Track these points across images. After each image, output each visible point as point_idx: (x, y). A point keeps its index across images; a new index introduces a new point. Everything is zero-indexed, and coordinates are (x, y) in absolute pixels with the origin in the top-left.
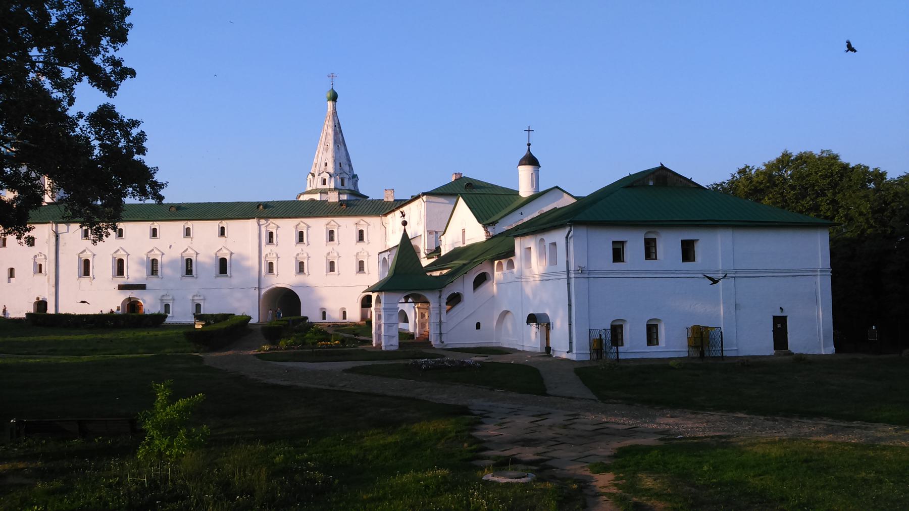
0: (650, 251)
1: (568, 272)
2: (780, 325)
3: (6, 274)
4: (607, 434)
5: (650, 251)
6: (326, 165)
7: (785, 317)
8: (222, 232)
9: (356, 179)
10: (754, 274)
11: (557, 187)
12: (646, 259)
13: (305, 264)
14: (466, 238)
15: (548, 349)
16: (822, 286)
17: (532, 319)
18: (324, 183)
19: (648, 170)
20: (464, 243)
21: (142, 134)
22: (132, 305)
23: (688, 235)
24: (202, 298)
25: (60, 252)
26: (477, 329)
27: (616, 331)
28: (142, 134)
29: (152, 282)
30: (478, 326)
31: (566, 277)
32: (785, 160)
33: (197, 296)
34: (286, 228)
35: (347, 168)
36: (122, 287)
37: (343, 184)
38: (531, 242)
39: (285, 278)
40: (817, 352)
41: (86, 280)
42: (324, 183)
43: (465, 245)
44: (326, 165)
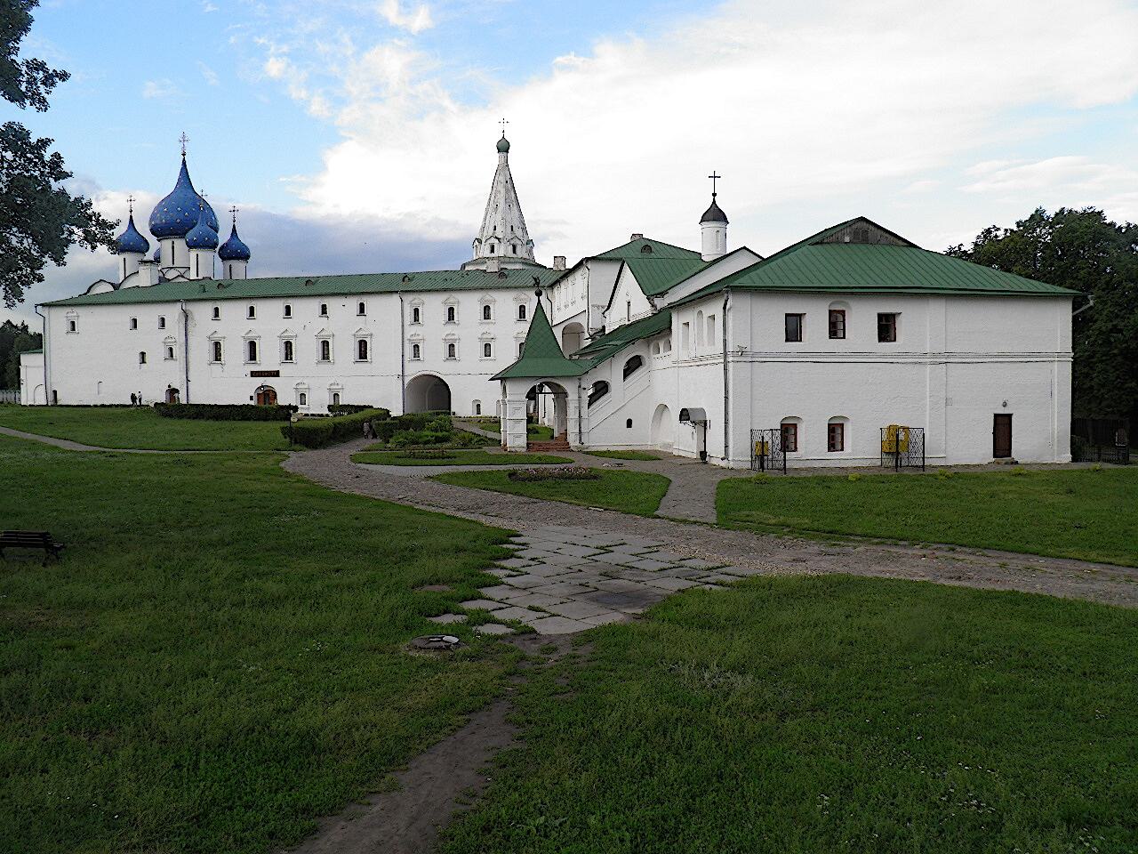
0: (836, 328)
1: (725, 354)
2: (1003, 425)
3: (138, 358)
5: (836, 328)
6: (495, 229)
7: (1010, 416)
8: (288, 310)
9: (531, 245)
10: (968, 360)
11: (745, 248)
12: (830, 338)
13: (76, 323)
14: (632, 314)
15: (703, 454)
16: (1060, 377)
17: (685, 415)
18: (492, 251)
21: (57, 156)
22: (267, 394)
23: (888, 307)
24: (306, 386)
25: (190, 334)
27: (788, 432)
28: (57, 156)
29: (284, 370)
30: (629, 423)
32: (1038, 218)
33: (334, 384)
34: (433, 306)
35: (519, 233)
36: (254, 374)
37: (514, 252)
38: (690, 316)
39: (433, 363)
40: (1056, 460)
41: (216, 367)
42: (492, 251)
44: (495, 229)
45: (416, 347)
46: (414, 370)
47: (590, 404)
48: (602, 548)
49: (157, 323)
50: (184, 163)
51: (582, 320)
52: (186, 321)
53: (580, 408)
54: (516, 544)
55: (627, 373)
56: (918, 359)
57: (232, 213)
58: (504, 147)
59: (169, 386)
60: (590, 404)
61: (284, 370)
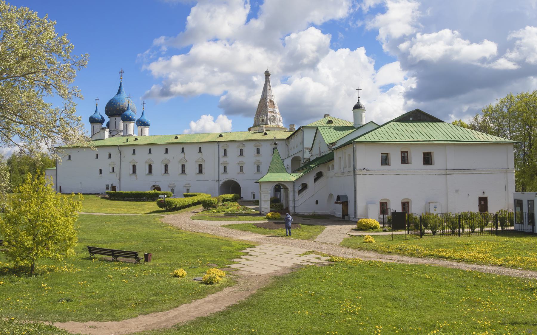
3: (98, 172)
4: (313, 263)
11: (372, 122)
12: (402, 163)
19: (411, 112)
20: (320, 155)
26: (316, 204)
30: (317, 202)
31: (353, 174)
43: (321, 156)
45: (225, 168)
46: (224, 178)
47: (299, 194)
48: (304, 260)
49: (108, 156)
50: (121, 82)
51: (301, 155)
52: (120, 155)
53: (294, 195)
54: (412, 255)
55: (316, 180)
56: (446, 172)
58: (122, 72)
60: (299, 194)
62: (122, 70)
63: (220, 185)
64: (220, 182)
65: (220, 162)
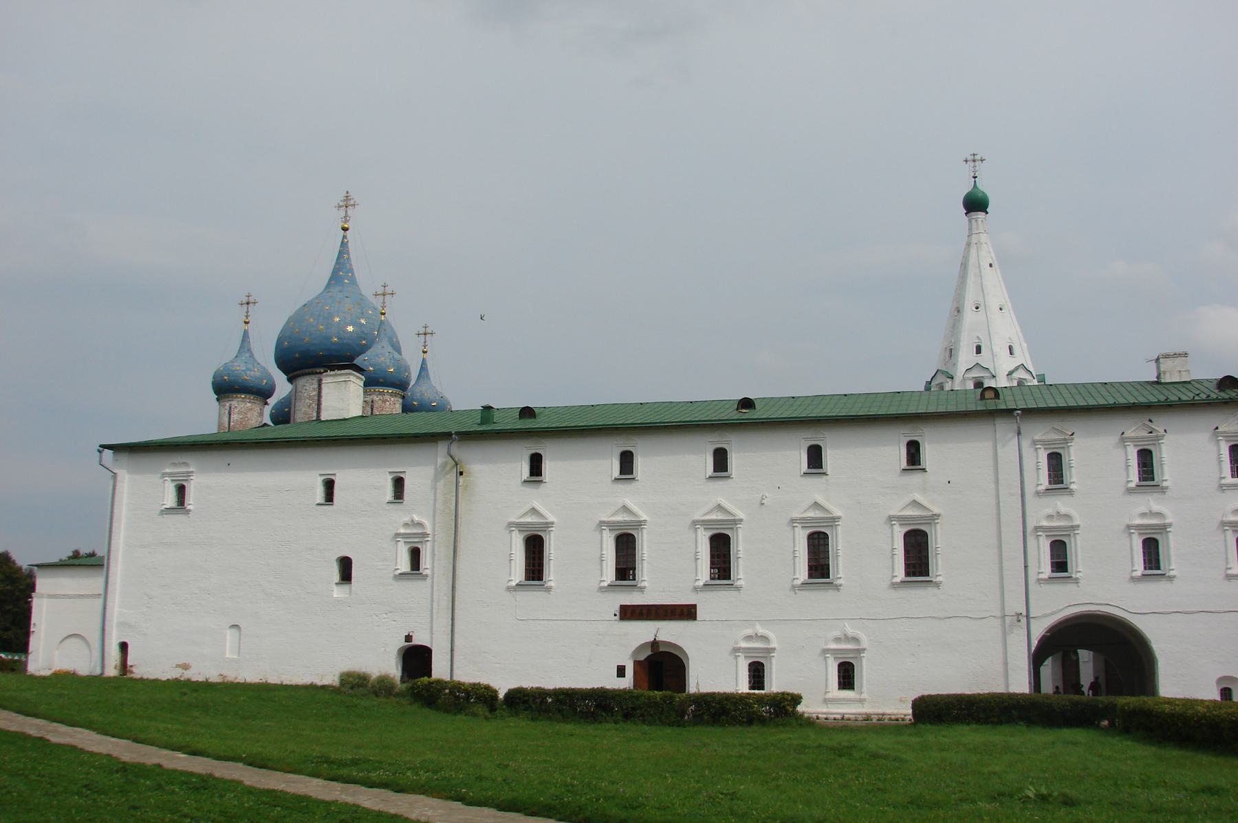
12: (618, 677)
29: (710, 605)
57: (381, 298)
58: (347, 203)
59: (408, 638)
61: (710, 605)
62: (347, 198)
63: (1035, 643)
64: (1033, 623)
65: (1031, 525)
